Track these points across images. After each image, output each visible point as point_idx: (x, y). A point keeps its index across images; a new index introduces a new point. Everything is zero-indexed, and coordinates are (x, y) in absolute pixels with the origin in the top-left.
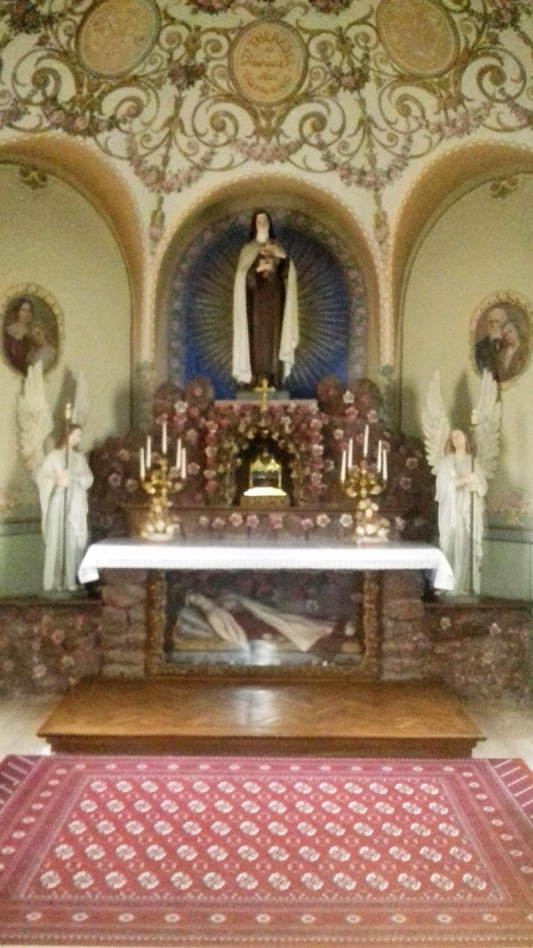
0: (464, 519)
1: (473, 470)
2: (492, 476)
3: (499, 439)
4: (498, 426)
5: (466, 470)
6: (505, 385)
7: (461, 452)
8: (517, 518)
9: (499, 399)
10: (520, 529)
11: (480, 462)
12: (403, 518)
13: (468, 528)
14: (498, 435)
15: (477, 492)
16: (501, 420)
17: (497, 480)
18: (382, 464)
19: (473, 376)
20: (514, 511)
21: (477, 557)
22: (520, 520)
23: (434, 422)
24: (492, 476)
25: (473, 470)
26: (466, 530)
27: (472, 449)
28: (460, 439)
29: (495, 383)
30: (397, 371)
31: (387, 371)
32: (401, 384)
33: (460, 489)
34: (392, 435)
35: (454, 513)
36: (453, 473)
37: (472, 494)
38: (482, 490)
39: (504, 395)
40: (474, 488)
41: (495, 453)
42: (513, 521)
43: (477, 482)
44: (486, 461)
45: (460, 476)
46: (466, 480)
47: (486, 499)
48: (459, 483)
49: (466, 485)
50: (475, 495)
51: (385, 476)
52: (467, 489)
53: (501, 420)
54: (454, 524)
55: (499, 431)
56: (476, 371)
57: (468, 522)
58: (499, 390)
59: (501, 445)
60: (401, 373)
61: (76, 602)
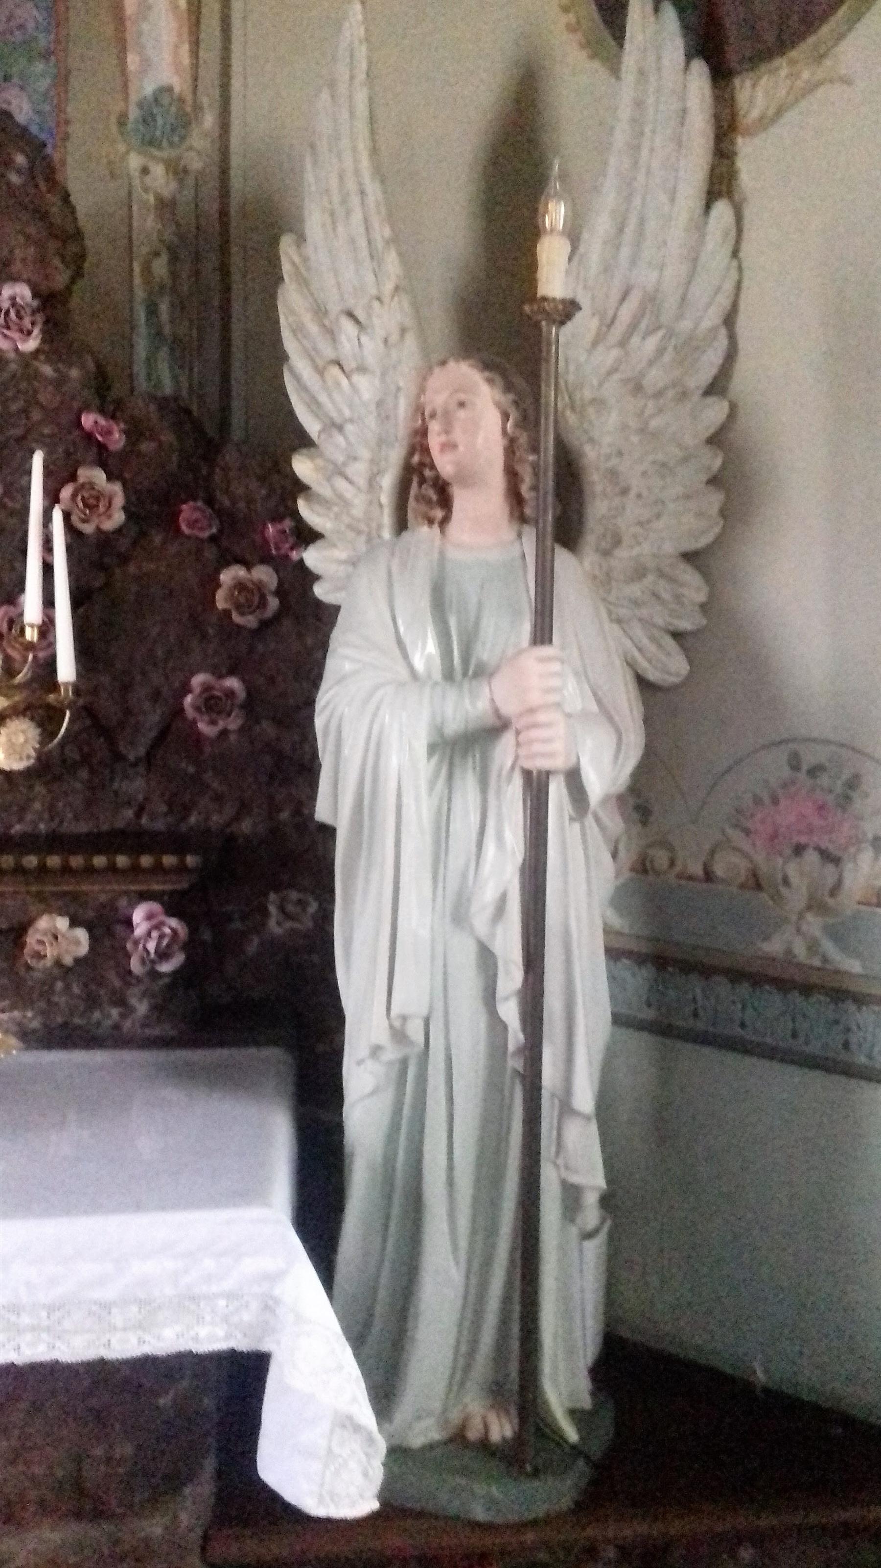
0: (487, 959)
1: (542, 634)
2: (672, 666)
3: (717, 439)
4: (710, 361)
5: (504, 630)
6: (755, 93)
7: (481, 515)
8: (814, 924)
9: (721, 183)
10: (841, 994)
11: (603, 582)
12: (174, 905)
13: (510, 1012)
14: (715, 412)
15: (574, 778)
16: (729, 320)
17: (697, 705)
18: (49, 602)
19: (574, 77)
20: (802, 874)
21: (572, 1196)
22: (836, 935)
23: (357, 361)
24: (672, 666)
25: (542, 634)
26: (497, 1025)
27: (557, 500)
28: (478, 426)
29: (699, 79)
30: (209, 120)
31: (160, 123)
32: (224, 192)
33: (465, 748)
34: (136, 431)
35: (418, 919)
36: (426, 652)
37: (536, 787)
38: (605, 764)
39: (749, 153)
40: (550, 749)
41: (689, 522)
42: (790, 941)
43: (577, 716)
44: (639, 573)
45: (464, 666)
46: (500, 694)
47: (640, 800)
48: (466, 708)
49: (496, 728)
50: (557, 791)
51: (66, 670)
52: (504, 752)
53: (729, 320)
54: (413, 994)
55: (717, 387)
56: (587, 44)
57: (511, 978)
58: (726, 130)
59: (732, 474)
60: (225, 126)
61: (331, 706)
